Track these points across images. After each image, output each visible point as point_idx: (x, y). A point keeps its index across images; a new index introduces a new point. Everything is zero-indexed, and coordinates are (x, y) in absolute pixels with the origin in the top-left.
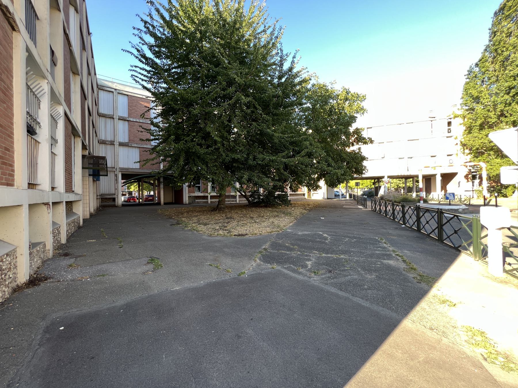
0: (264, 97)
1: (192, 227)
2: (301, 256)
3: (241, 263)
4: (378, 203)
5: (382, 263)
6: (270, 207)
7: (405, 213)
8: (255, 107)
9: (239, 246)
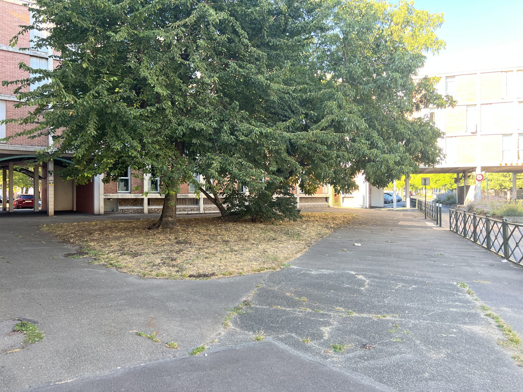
0: (252, 12)
1: (107, 260)
2: (313, 317)
3: (198, 331)
4: (461, 218)
5: (460, 331)
6: (261, 222)
7: (508, 237)
8: (235, 32)
9: (197, 297)
